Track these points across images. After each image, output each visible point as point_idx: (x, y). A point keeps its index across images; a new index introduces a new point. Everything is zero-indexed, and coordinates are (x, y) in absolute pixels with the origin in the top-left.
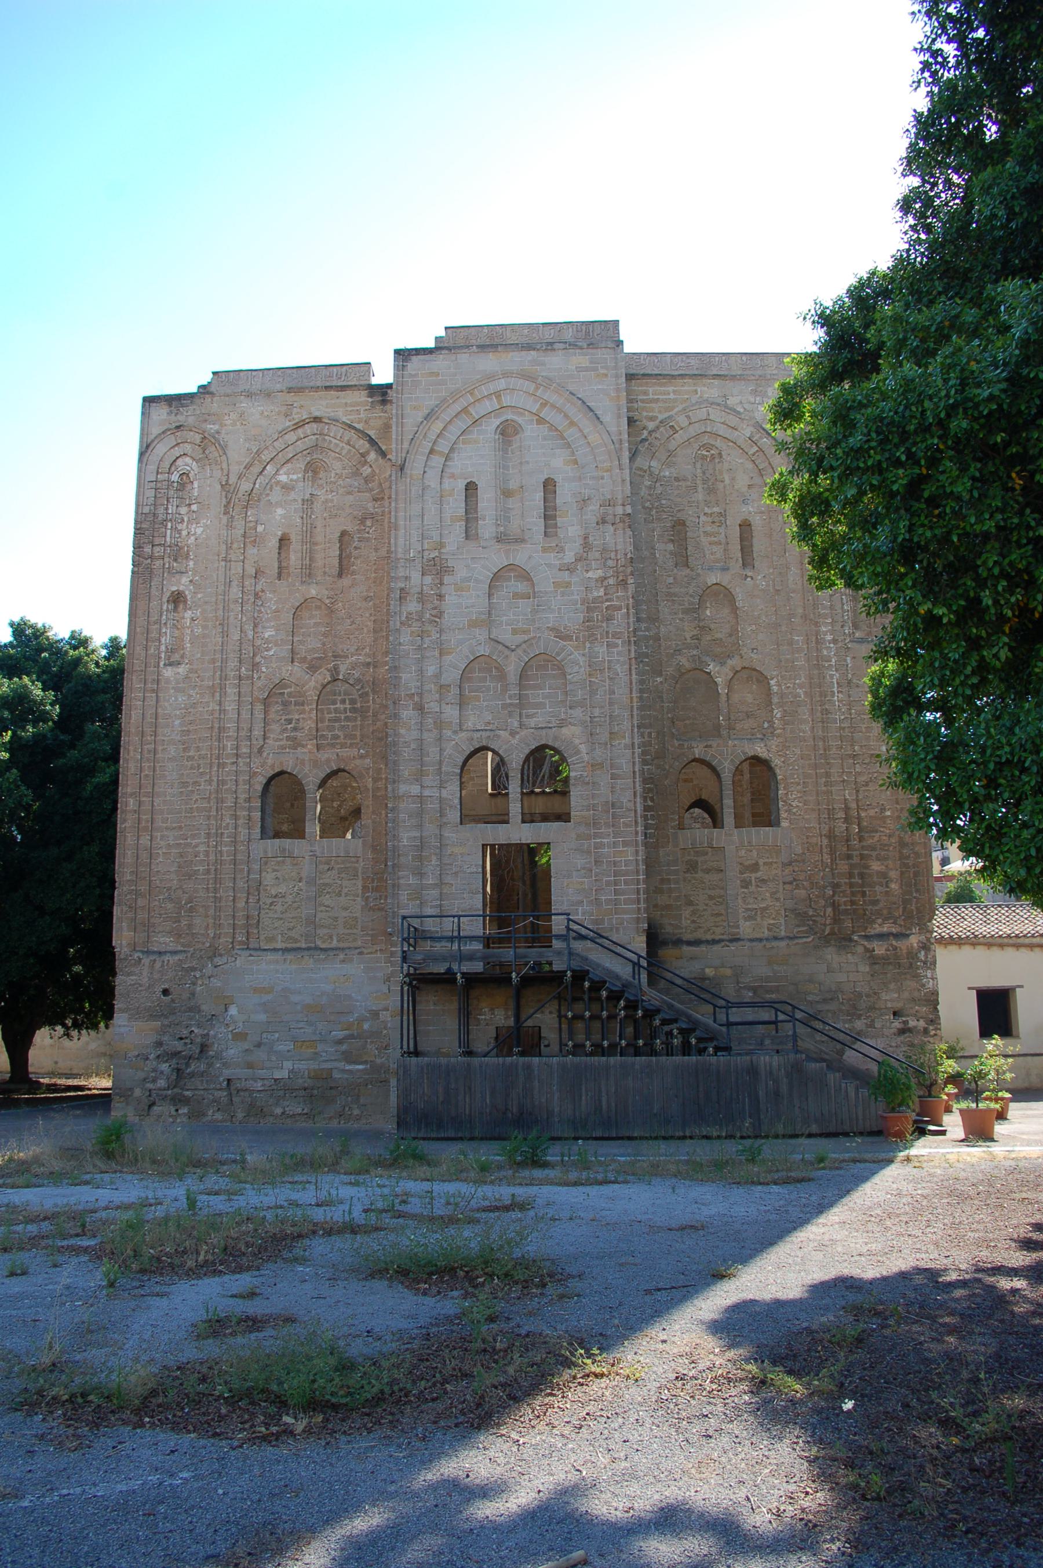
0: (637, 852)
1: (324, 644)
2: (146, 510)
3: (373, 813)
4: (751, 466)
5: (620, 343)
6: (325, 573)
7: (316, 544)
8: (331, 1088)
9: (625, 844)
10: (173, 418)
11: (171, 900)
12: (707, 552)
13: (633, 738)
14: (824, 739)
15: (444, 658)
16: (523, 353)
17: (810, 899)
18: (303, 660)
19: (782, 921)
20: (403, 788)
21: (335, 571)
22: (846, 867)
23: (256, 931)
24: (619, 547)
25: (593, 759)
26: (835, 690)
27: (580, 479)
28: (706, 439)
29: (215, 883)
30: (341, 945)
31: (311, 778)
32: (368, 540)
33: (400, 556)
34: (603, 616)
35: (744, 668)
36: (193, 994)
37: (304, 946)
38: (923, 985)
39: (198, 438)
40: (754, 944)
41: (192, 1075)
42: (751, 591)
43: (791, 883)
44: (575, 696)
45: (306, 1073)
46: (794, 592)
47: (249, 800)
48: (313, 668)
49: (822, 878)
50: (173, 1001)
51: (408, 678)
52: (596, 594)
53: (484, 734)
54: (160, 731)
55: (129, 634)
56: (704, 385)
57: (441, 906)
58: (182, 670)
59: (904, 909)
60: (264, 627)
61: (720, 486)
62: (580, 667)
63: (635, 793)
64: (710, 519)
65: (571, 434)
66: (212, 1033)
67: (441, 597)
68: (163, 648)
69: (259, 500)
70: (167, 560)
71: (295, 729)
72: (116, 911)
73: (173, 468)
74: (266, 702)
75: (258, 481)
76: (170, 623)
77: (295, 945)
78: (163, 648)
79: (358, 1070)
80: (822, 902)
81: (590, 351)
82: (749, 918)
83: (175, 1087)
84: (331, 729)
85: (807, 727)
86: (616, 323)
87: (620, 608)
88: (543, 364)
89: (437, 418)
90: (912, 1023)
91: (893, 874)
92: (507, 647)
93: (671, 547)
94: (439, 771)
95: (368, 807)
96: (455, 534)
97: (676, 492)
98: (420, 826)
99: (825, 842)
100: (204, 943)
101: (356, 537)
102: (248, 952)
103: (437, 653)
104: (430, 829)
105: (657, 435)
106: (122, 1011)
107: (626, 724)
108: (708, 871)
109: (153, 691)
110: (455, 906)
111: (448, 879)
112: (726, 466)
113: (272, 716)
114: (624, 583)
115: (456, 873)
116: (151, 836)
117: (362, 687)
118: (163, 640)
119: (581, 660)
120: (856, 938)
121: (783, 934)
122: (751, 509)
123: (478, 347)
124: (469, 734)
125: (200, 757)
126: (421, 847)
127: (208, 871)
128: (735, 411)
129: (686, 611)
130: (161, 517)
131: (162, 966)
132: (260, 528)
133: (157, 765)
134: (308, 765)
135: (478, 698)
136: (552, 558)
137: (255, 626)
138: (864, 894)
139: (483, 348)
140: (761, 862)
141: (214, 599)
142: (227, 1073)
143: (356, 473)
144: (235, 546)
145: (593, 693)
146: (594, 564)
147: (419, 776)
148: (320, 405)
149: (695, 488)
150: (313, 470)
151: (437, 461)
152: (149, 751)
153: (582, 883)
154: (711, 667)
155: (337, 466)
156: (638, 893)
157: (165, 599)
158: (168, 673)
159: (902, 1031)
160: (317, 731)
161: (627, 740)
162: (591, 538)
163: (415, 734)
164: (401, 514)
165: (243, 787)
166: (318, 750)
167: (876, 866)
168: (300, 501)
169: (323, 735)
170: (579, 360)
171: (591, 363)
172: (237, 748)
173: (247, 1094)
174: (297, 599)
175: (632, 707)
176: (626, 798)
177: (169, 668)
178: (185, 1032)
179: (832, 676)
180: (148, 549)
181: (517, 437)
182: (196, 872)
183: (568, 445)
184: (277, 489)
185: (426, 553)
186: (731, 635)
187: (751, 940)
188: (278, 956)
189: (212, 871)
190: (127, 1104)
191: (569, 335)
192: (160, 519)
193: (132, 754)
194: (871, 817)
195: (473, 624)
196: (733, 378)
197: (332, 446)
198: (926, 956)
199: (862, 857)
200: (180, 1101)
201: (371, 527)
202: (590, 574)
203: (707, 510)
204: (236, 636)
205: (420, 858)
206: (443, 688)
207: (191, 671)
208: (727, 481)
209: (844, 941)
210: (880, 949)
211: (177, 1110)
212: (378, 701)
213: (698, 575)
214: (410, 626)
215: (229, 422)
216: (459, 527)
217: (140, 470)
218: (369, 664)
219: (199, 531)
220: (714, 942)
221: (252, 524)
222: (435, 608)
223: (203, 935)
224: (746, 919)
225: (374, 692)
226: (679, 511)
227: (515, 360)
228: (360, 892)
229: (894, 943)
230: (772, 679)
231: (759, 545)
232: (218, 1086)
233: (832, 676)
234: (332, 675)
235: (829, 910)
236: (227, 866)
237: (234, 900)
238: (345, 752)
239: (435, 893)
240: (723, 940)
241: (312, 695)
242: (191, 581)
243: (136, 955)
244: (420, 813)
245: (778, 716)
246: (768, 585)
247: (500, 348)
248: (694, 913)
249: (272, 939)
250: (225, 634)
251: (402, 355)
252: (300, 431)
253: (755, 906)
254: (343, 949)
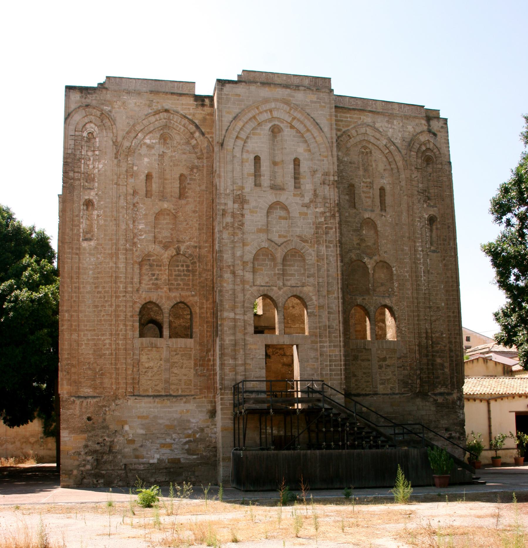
0: (340, 350)
1: (172, 234)
2: (70, 151)
3: (200, 325)
4: (385, 159)
5: (332, 91)
6: (171, 196)
7: (166, 179)
8: (180, 468)
9: (335, 346)
10: (83, 100)
11: (90, 369)
12: (364, 201)
13: (338, 294)
14: (417, 298)
15: (245, 247)
16: (284, 90)
17: (410, 375)
18: (161, 242)
19: (397, 386)
20: (226, 314)
21: (177, 195)
22: (426, 360)
23: (137, 386)
24: (331, 197)
25: (319, 303)
26: (422, 275)
27: (312, 160)
28: (364, 144)
29: (116, 360)
30: (183, 394)
31: (166, 306)
32: (195, 180)
33: (222, 192)
34: (323, 231)
35: (381, 261)
36: (105, 419)
37: (163, 394)
38: (459, 417)
39: (98, 113)
40: (385, 396)
41: (105, 462)
42: (384, 222)
43: (401, 367)
44: (310, 271)
45: (167, 461)
46: (404, 225)
47: (132, 316)
48: (166, 247)
49: (416, 366)
50: (93, 423)
51: (227, 257)
52: (320, 220)
53: (266, 288)
54: (81, 276)
56: (364, 116)
57: (245, 375)
58: (92, 243)
59: (451, 381)
60: (138, 223)
61: (371, 168)
62: (312, 257)
63: (339, 321)
64: (365, 185)
65: (307, 136)
66: (116, 440)
67: (243, 215)
68: (81, 230)
69: (134, 152)
70: (82, 181)
71: (157, 279)
72: (60, 374)
73: (84, 129)
74: (141, 264)
75: (134, 142)
76: (85, 216)
77: (158, 394)
78: (81, 230)
79: (194, 459)
80: (416, 377)
81: (318, 93)
82: (383, 384)
83: (96, 469)
84: (176, 280)
85: (409, 292)
86: (330, 79)
87: (332, 228)
88: (293, 97)
89: (240, 120)
90: (453, 435)
91: (447, 364)
92: (276, 244)
93: (347, 197)
94: (243, 306)
95: (196, 322)
96: (249, 183)
97: (350, 170)
98: (234, 334)
99: (417, 348)
100: (110, 393)
101: (189, 177)
102: (134, 398)
103: (241, 245)
104: (239, 336)
105: (342, 139)
106: (65, 429)
107: (335, 287)
108: (363, 360)
109: (77, 254)
110: (252, 375)
111: (248, 361)
112: (374, 158)
113: (144, 271)
114: (333, 216)
115: (252, 359)
116: (78, 334)
117: (193, 259)
118: (81, 226)
119: (313, 253)
120: (430, 394)
121: (397, 392)
122: (385, 182)
123: (261, 83)
124: (258, 288)
125: (105, 292)
126: (235, 345)
127: (112, 354)
128: (378, 130)
129: (354, 231)
130: (78, 157)
131: (87, 405)
132: (135, 168)
133: (80, 295)
134: (165, 299)
135: (262, 270)
136: (298, 199)
137: (134, 222)
138: (433, 374)
139: (263, 84)
140: (387, 357)
141: (110, 206)
142: (124, 461)
143: (188, 143)
144: (122, 176)
145: (319, 270)
146: (319, 205)
147: (233, 309)
148: (169, 103)
149: (359, 168)
150: (164, 138)
151: (240, 143)
152: (76, 288)
153: (314, 365)
154: (366, 260)
155: (177, 137)
156: (341, 371)
157: (82, 203)
158: (85, 244)
160: (169, 280)
161: (335, 295)
162: (318, 191)
163: (231, 286)
164: (222, 170)
165: (129, 309)
166: (170, 291)
167: (439, 360)
168: (157, 155)
169: (172, 283)
170: (311, 97)
171: (318, 99)
172: (126, 288)
173: (135, 472)
174: (156, 209)
175: (338, 279)
176: (335, 324)
177: (86, 242)
178: (101, 440)
179: (421, 268)
180: (71, 174)
181: (280, 134)
182: (105, 354)
183: (306, 141)
184: (144, 147)
185: (235, 192)
186: (374, 244)
187: (384, 394)
188: (151, 399)
189: (114, 354)
190: (70, 478)
191: (306, 82)
192: (77, 157)
193: (66, 288)
194: (437, 337)
195: (260, 231)
196: (378, 113)
197: (175, 127)
198: (460, 403)
199: (433, 356)
200: (99, 476)
201: (196, 173)
202: (317, 210)
203: (364, 180)
204: (123, 227)
205: (235, 350)
206: (245, 263)
207: (98, 244)
208: (374, 166)
209: (423, 395)
210: (440, 399)
211: (97, 481)
212: (202, 267)
213: (360, 213)
214: (228, 229)
215: (116, 106)
216: (251, 179)
217: (65, 128)
218: (196, 247)
219: (101, 166)
220: (366, 395)
221: (131, 165)
222: (240, 221)
223: (109, 388)
224: (381, 384)
225: (199, 261)
226: (351, 179)
227: (281, 93)
228: (193, 366)
229: (446, 397)
230: (394, 267)
231: (389, 199)
232: (120, 468)
233: (421, 268)
234: (177, 252)
235: (418, 381)
236: (122, 351)
237: (126, 370)
238: (184, 293)
239: (242, 368)
240: (371, 394)
241: (166, 261)
242: (96, 194)
243: (72, 399)
244: (235, 327)
245: (396, 286)
246: (392, 221)
247: (272, 86)
248: (356, 380)
249: (147, 390)
250: (118, 225)
251: (221, 83)
252: (157, 116)
253: (385, 378)
254: (185, 396)
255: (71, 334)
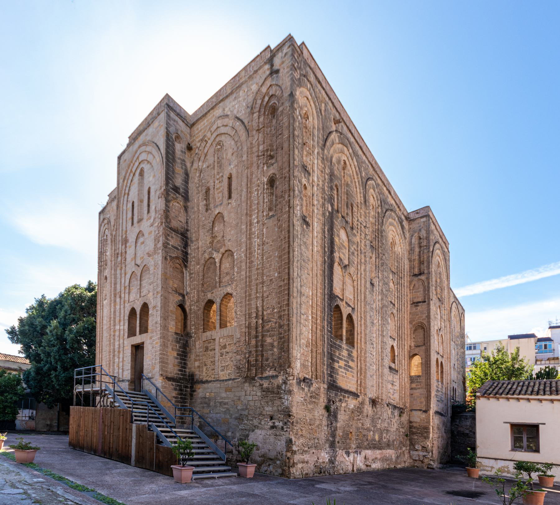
38: (283, 403)
55: (98, 281)
90: (277, 424)
91: (276, 344)
159: (273, 427)
167: (269, 340)
209: (250, 379)
255: (331, 462)
